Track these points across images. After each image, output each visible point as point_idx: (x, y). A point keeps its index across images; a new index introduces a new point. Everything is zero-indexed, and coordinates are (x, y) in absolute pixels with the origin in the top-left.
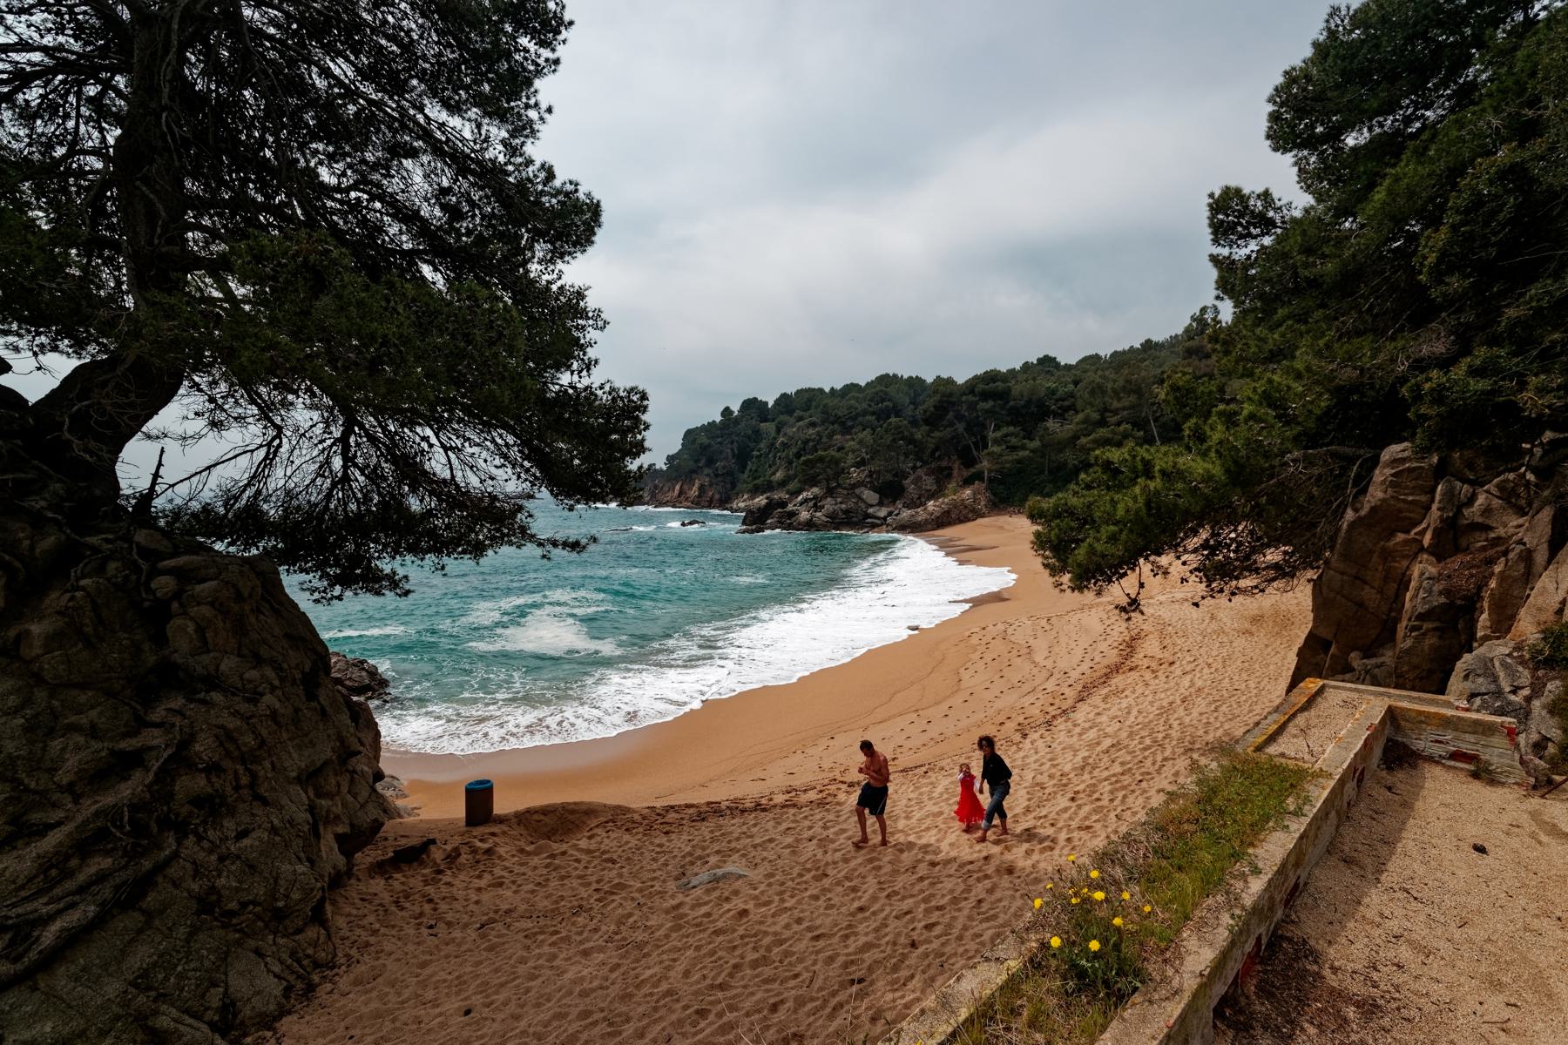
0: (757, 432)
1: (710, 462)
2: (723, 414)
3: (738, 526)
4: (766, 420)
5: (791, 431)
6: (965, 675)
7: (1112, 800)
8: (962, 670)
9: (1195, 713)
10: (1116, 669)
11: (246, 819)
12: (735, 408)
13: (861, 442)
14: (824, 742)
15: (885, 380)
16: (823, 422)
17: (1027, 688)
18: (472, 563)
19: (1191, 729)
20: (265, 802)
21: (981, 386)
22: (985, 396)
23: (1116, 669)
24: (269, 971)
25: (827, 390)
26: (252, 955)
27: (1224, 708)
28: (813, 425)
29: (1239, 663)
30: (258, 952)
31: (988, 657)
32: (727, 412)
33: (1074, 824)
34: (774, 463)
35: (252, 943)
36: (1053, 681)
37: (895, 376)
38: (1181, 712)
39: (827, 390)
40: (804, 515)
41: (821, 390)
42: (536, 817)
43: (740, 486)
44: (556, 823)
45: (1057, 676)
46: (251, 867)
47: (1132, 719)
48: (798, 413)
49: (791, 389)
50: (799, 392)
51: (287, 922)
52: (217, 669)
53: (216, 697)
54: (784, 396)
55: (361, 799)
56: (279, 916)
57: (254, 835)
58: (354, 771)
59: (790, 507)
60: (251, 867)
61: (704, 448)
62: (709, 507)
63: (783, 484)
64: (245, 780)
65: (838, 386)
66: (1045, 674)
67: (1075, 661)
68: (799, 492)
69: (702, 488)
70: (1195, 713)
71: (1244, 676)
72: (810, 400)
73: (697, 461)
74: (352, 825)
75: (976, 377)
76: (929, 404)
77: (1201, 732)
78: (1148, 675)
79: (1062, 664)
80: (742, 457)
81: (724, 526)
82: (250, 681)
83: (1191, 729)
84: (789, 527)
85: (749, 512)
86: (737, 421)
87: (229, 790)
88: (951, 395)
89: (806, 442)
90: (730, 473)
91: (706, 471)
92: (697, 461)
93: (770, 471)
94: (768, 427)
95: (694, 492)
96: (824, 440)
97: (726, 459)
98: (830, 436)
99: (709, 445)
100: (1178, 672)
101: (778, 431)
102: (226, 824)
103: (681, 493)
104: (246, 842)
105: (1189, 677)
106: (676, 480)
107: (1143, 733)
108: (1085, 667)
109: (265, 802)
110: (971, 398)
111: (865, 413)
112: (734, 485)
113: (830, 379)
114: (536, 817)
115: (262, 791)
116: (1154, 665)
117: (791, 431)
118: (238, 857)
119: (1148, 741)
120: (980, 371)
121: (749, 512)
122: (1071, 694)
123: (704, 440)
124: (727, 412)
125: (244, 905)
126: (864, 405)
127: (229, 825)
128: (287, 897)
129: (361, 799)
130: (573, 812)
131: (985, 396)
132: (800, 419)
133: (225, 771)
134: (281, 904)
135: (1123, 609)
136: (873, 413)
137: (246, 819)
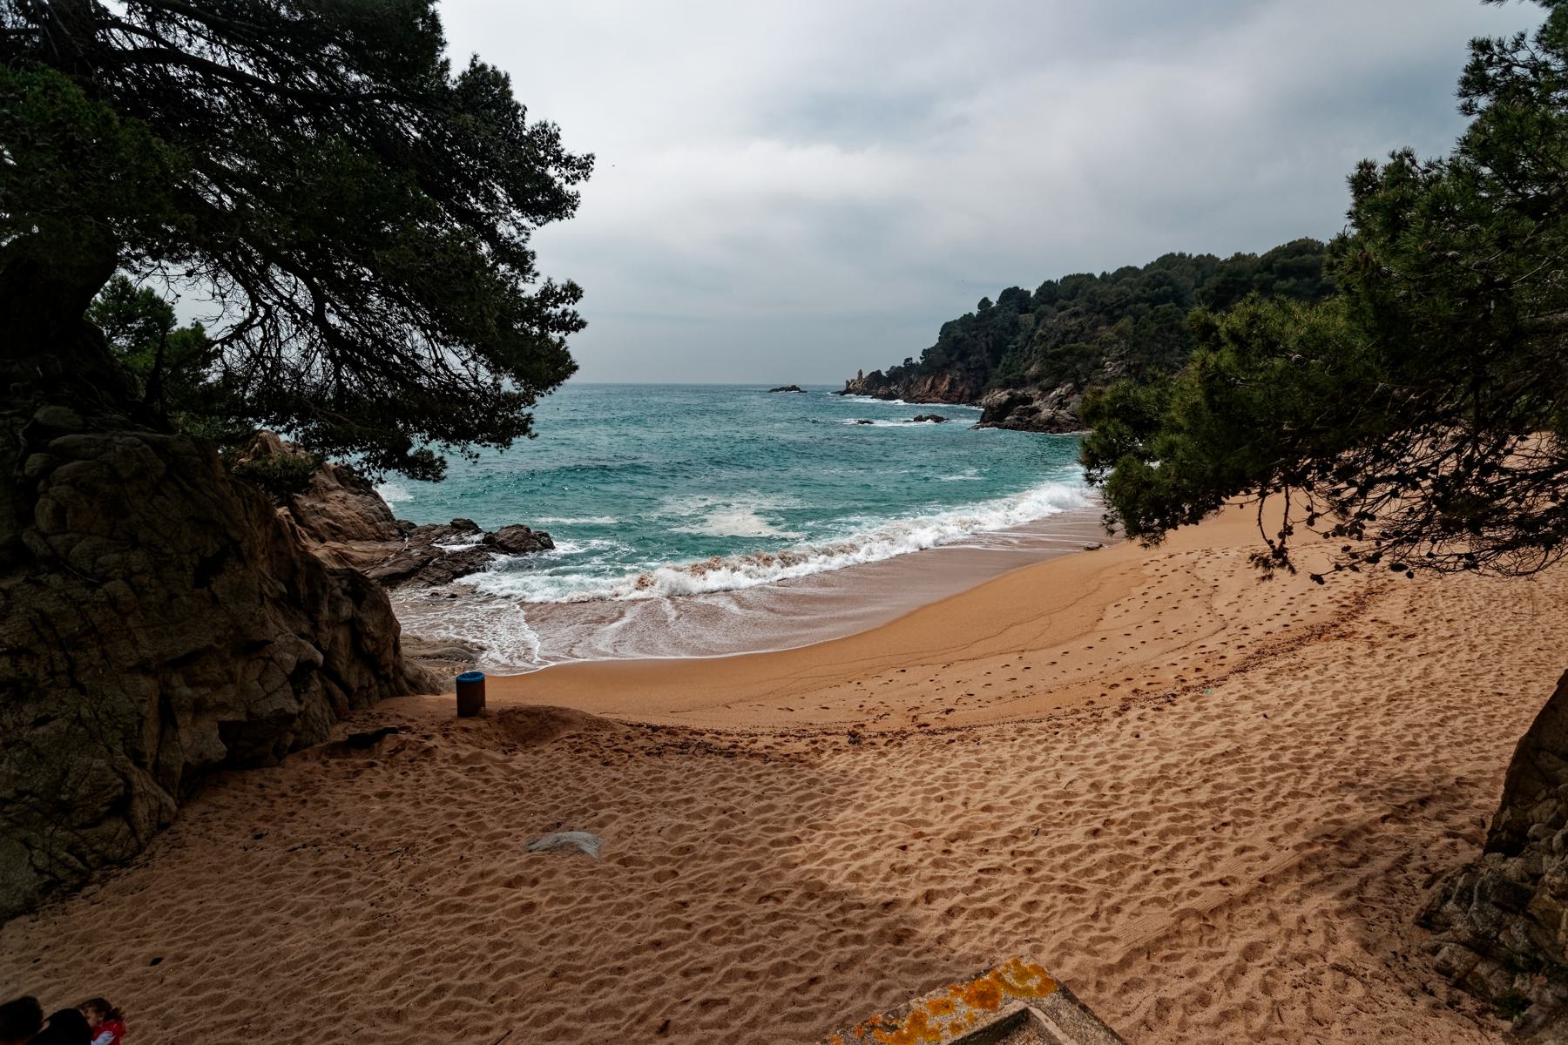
0: (1015, 324)
1: (963, 356)
2: (980, 306)
3: (974, 422)
4: (1026, 311)
5: (1050, 322)
6: (1111, 612)
7: (1152, 849)
8: (1111, 607)
9: (1398, 724)
10: (1319, 633)
11: (52, 706)
12: (994, 299)
13: (1120, 333)
14: (892, 674)
15: (1168, 261)
16: (1088, 311)
17: (1180, 641)
18: (497, 452)
19: (1376, 749)
20: (82, 690)
21: (1282, 260)
22: (1285, 272)
23: (1319, 633)
24: (31, 863)
25: (1098, 276)
26: (17, 845)
27: (1459, 723)
28: (1076, 314)
29: (1530, 651)
30: (27, 843)
31: (1153, 595)
32: (985, 303)
33: (1060, 877)
34: (1029, 357)
35: (23, 833)
36: (1222, 636)
37: (1182, 255)
38: (1378, 716)
39: (1098, 276)
40: (1046, 413)
41: (1091, 276)
42: (519, 718)
43: (992, 381)
44: (532, 726)
45: (1230, 630)
46: (39, 756)
47: (1288, 715)
48: (1061, 302)
49: (1056, 277)
50: (1065, 279)
51: (73, 815)
52: (68, 551)
53: (55, 580)
54: (1048, 284)
55: (269, 688)
56: (66, 808)
57: (52, 724)
58: (272, 659)
59: (1036, 404)
60: (39, 756)
61: (958, 341)
62: (958, 403)
63: (1036, 379)
64: (62, 667)
65: (1111, 271)
66: (1218, 624)
67: (1268, 613)
68: (1053, 389)
69: (952, 383)
70: (1398, 724)
71: (1529, 673)
72: (1076, 288)
73: (949, 355)
74: (249, 714)
75: (1278, 250)
76: (1213, 281)
77: (1388, 758)
78: (1361, 648)
79: (1246, 616)
80: (997, 350)
81: (964, 421)
82: (101, 566)
83: (1376, 749)
84: (1027, 427)
85: (988, 408)
86: (994, 312)
87: (41, 674)
88: (1239, 273)
89: (1066, 334)
90: (983, 368)
91: (959, 365)
92: (949, 355)
93: (1024, 365)
94: (1028, 319)
95: (944, 386)
96: (1087, 331)
97: (980, 352)
98: (1094, 327)
99: (963, 339)
100: (1413, 652)
101: (1037, 324)
102: (26, 709)
103: (933, 387)
104: (41, 730)
105: (1424, 662)
106: (928, 374)
107: (1290, 741)
108: (1276, 625)
109: (82, 690)
110: (1266, 275)
111: (1138, 299)
112: (986, 380)
113: (1100, 264)
114: (519, 718)
115: (82, 679)
116: (1380, 636)
117: (1050, 322)
118: (28, 744)
119: (1286, 758)
120: (1283, 241)
121: (988, 408)
122: (1233, 656)
123: (959, 333)
124: (985, 303)
125: (21, 794)
126: (1138, 291)
127: (30, 711)
128: (73, 790)
129: (269, 688)
130: (554, 718)
131: (1285, 272)
132: (1063, 308)
133: (38, 656)
134: (64, 797)
135: (1265, 563)
136: (1147, 300)
137: (52, 706)
